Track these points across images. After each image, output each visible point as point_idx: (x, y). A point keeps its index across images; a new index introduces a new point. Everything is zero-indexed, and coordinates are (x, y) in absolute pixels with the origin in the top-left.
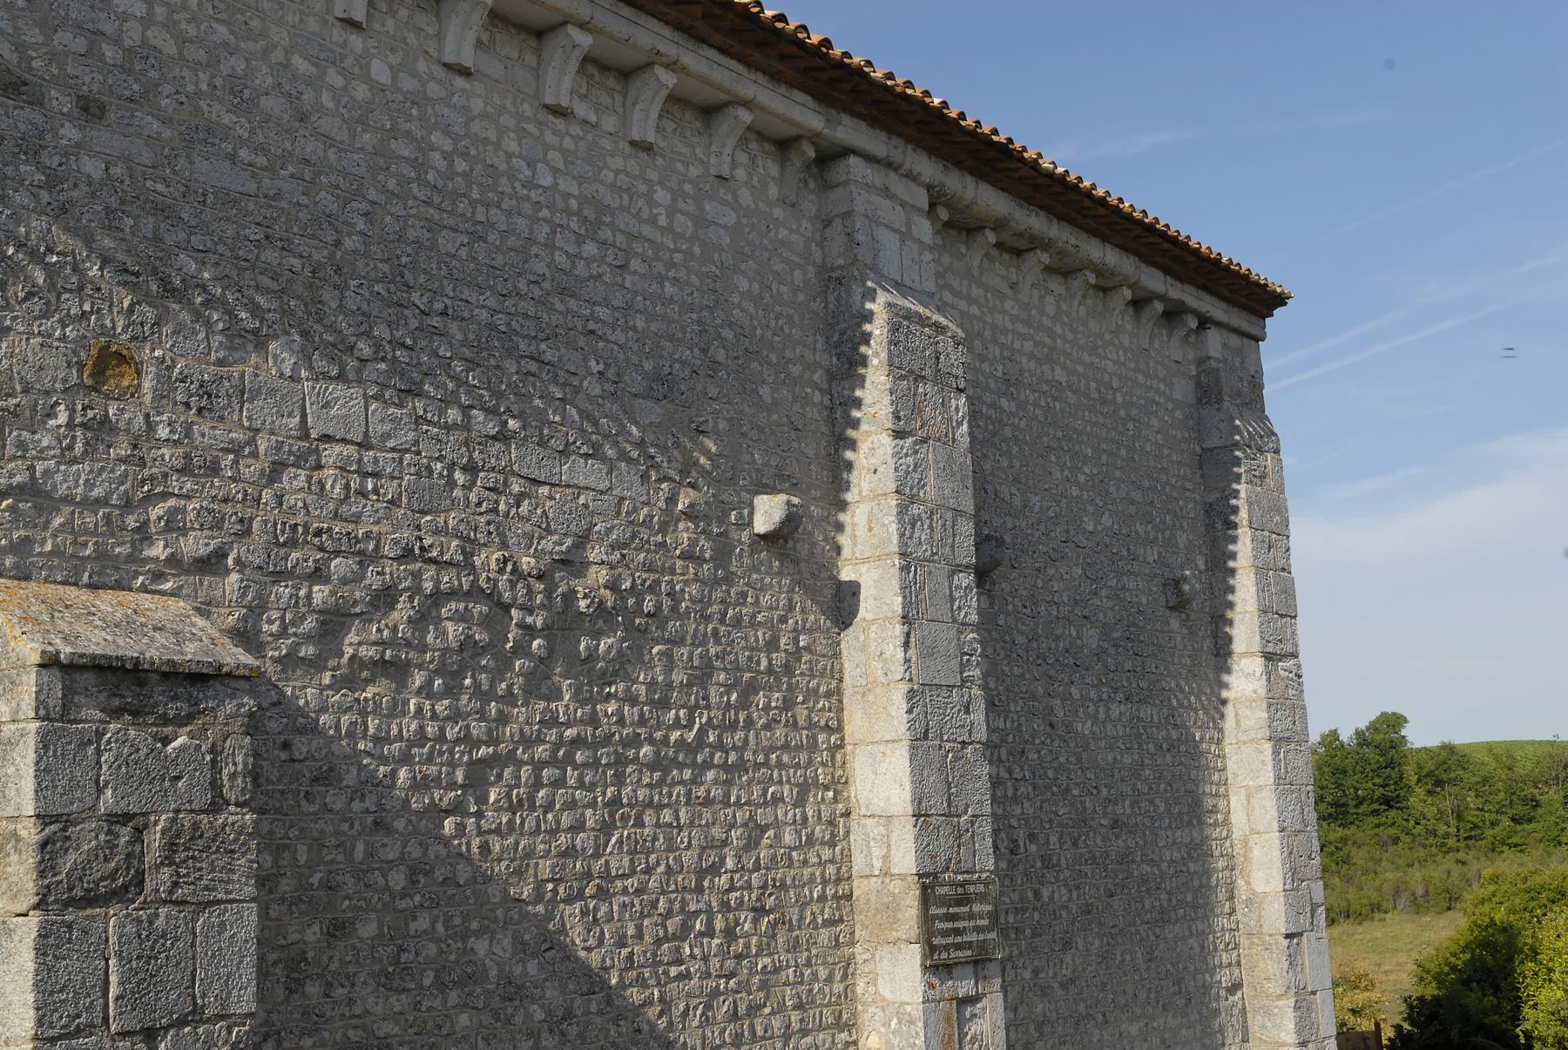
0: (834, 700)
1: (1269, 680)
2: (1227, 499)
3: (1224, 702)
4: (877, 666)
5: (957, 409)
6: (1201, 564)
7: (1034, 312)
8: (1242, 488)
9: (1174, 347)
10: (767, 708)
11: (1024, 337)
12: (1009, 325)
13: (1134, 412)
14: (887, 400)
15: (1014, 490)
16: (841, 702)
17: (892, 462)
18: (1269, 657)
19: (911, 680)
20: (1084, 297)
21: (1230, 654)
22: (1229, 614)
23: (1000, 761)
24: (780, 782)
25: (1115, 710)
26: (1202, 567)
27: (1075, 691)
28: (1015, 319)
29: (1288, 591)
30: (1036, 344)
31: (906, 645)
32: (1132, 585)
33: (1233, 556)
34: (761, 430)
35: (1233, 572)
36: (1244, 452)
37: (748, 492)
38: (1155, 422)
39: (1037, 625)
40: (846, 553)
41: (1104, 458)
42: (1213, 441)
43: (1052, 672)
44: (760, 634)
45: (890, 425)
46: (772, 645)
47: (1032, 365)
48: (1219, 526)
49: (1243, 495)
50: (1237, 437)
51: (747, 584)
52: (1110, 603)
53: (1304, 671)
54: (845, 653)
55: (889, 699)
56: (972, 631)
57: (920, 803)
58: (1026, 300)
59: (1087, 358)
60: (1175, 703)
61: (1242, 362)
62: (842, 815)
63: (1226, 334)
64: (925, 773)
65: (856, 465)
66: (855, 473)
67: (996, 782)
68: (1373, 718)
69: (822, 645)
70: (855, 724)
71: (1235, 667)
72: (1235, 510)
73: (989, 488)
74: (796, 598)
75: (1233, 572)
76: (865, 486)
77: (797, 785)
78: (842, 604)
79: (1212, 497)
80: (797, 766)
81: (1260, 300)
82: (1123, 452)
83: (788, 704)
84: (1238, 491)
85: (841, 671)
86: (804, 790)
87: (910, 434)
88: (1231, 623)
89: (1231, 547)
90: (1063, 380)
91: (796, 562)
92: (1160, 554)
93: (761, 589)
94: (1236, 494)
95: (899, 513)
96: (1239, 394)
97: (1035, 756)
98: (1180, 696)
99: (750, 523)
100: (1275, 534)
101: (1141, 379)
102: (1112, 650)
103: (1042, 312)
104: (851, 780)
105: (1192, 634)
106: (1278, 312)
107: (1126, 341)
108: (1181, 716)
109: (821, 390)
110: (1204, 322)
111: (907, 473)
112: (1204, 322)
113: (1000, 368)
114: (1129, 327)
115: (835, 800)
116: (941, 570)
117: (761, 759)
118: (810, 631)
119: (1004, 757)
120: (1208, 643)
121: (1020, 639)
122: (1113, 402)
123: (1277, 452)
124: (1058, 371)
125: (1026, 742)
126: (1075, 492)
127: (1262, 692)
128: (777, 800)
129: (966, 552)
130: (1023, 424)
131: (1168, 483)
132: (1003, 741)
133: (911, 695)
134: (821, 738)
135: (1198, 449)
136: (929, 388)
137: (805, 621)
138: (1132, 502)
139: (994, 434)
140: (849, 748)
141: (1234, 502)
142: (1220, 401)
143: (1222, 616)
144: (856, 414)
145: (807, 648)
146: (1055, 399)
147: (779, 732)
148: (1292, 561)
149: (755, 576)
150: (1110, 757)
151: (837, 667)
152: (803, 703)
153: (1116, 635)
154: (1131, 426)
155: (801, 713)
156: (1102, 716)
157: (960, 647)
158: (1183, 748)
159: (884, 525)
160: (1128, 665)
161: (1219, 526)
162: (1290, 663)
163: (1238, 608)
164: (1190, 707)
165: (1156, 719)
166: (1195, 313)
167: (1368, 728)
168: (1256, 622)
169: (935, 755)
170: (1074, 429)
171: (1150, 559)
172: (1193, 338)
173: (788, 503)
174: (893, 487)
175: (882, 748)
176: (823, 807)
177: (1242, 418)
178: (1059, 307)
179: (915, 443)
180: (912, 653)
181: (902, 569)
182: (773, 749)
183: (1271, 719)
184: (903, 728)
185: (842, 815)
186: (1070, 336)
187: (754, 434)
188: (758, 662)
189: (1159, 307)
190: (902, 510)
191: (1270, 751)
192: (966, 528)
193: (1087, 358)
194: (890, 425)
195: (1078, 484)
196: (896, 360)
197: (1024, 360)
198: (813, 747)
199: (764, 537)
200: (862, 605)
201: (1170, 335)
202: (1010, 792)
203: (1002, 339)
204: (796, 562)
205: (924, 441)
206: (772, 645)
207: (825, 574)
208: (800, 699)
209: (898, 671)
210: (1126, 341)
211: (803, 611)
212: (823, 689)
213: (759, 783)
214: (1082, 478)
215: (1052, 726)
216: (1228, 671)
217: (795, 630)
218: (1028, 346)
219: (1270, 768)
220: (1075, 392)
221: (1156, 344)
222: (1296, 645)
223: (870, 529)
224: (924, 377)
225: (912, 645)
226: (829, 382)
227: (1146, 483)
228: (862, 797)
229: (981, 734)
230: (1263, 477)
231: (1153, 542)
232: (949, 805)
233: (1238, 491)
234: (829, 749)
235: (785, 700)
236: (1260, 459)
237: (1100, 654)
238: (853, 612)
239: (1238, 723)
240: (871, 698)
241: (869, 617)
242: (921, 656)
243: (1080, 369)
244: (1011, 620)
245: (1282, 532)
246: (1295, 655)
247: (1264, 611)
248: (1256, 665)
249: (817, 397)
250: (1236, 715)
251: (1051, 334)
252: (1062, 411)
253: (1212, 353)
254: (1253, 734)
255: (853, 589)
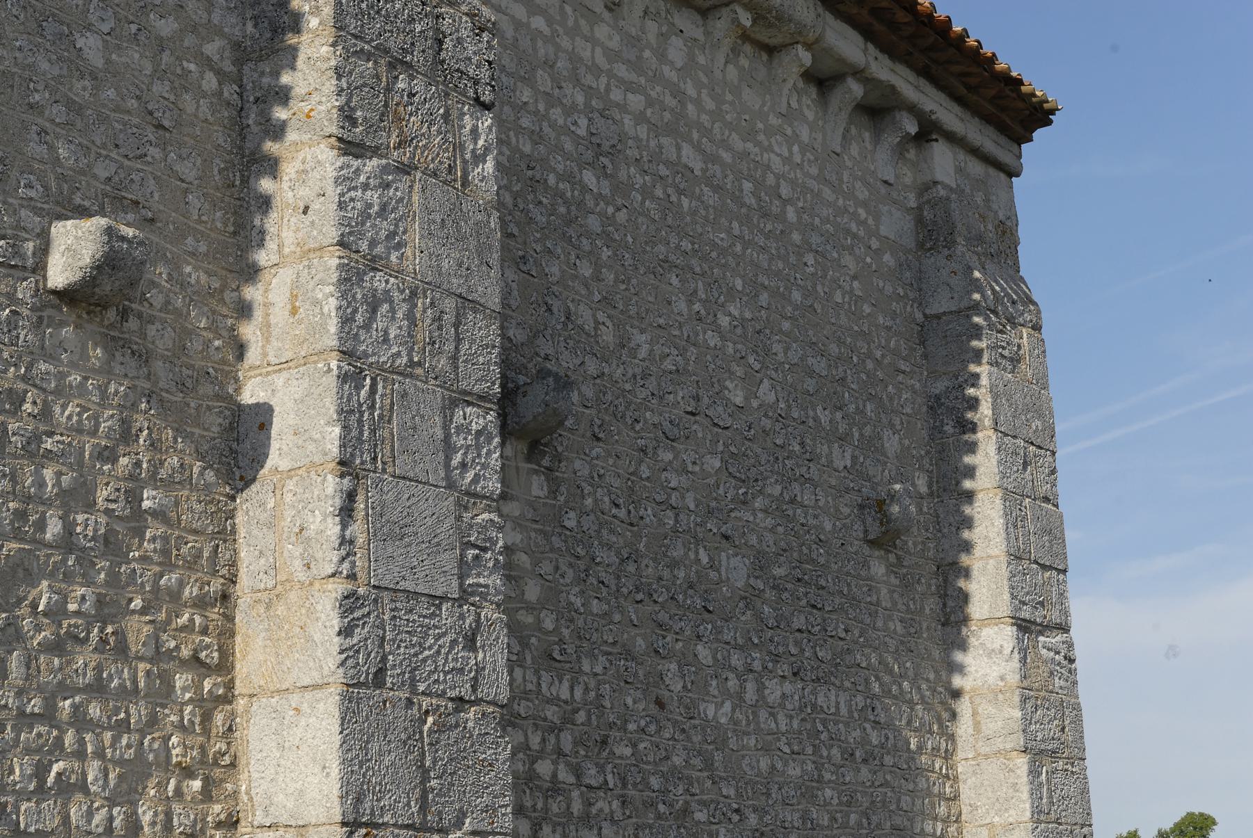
0: (214, 613)
1: (1023, 660)
2: (961, 387)
3: (957, 694)
4: (293, 551)
5: (475, 132)
6: (922, 485)
7: (647, 54)
8: (983, 370)
9: (877, 158)
10: (56, 613)
11: (630, 87)
12: (601, 60)
13: (815, 240)
14: (330, 85)
15: (601, 316)
16: (230, 619)
17: (333, 193)
18: (1024, 626)
19: (352, 577)
20: (735, 51)
21: (966, 620)
22: (964, 559)
23: (560, 753)
24: (80, 754)
25: (774, 691)
26: (924, 489)
27: (703, 652)
28: (613, 56)
29: (1054, 533)
30: (650, 103)
31: (346, 513)
32: (807, 498)
33: (970, 472)
34: (70, 105)
35: (969, 496)
36: (987, 318)
37: (37, 211)
38: (848, 260)
39: (638, 536)
40: (252, 356)
41: (764, 298)
42: (941, 304)
43: (663, 616)
44: (48, 474)
45: (334, 129)
46: (77, 497)
47: (642, 132)
48: (949, 429)
49: (984, 381)
50: (977, 296)
51: (24, 379)
52: (769, 522)
53: (1078, 653)
54: (242, 532)
55: (311, 611)
56: (488, 509)
57: (359, 800)
58: (633, 31)
59: (739, 145)
60: (876, 688)
61: (987, 201)
62: (219, 825)
63: (962, 156)
64: (374, 747)
65: (277, 202)
66: (274, 215)
67: (525, 781)
68: (1177, 819)
69: (192, 510)
70: (253, 660)
71: (973, 641)
72: (974, 404)
73: (556, 305)
74: (140, 421)
75: (969, 496)
76: (288, 236)
77: (121, 762)
78: (239, 445)
79: (939, 387)
80: (123, 726)
81: (1015, 112)
82: (797, 296)
83: (107, 609)
84: (977, 376)
85: (233, 564)
86: (133, 778)
87: (375, 151)
88: (966, 573)
89: (968, 459)
90: (697, 166)
91: (144, 358)
92: (854, 458)
93: (58, 392)
94: (974, 379)
95: (342, 281)
96: (980, 239)
97: (628, 751)
98: (887, 679)
99: (40, 267)
100: (1033, 447)
101: (828, 193)
102: (770, 594)
103: (662, 57)
104: (242, 761)
105: (907, 585)
106: (1039, 134)
107: (805, 135)
108: (886, 709)
109: (219, 73)
110: (928, 131)
111: (365, 215)
112: (928, 131)
113: (583, 122)
114: (810, 115)
115: (207, 795)
116: (431, 397)
117: (35, 705)
118: (168, 484)
119: (567, 747)
120: (931, 605)
121: (602, 555)
122: (781, 217)
123: (1037, 328)
124: (687, 150)
125: (611, 726)
126: (713, 340)
127: (1014, 679)
128: (68, 788)
129: (482, 372)
130: (622, 216)
131: (869, 355)
132: (568, 720)
133: (349, 603)
134: (181, 680)
135: (919, 316)
136: (418, 85)
137: (156, 466)
138: (811, 373)
139: (569, 222)
140: (241, 703)
141: (971, 391)
142: (950, 244)
143: (955, 564)
144: (281, 114)
145: (159, 514)
146: (681, 192)
147: (84, 659)
148: (1060, 488)
149: (43, 367)
150: (764, 764)
151: (224, 555)
152: (144, 611)
153: (779, 572)
154: (810, 259)
155: (138, 631)
156: (750, 695)
157: (462, 532)
158: (888, 760)
159: (316, 303)
160: (799, 622)
161: (949, 429)
162: (1057, 639)
163: (978, 551)
164: (900, 697)
165: (844, 711)
166: (913, 109)
167: (1173, 831)
168: (1005, 573)
169: (399, 718)
170: (714, 245)
171: (840, 464)
172: (912, 154)
173: (109, 231)
174: (333, 234)
175: (295, 699)
176: (177, 808)
177: (983, 269)
178: (691, 58)
179: (385, 170)
180: (357, 529)
181: (343, 378)
182: (65, 690)
183: (1027, 721)
184: (332, 662)
185: (219, 825)
186: (710, 104)
187: (58, 112)
188: (41, 525)
189: (856, 89)
190: (348, 279)
191: (1025, 769)
192: (483, 335)
193: (739, 145)
194: (334, 129)
195: (718, 329)
196: (353, 25)
197: (628, 122)
198: (163, 693)
199: (67, 296)
200: (275, 445)
201: (877, 140)
202: (577, 807)
203: (589, 80)
204: (144, 358)
205: (405, 169)
206: (77, 497)
207: (207, 389)
208: (137, 603)
209: (328, 559)
210: (805, 135)
211: (153, 445)
212: (189, 592)
213: (28, 751)
214: (724, 321)
215: (660, 704)
216: (963, 646)
217: (132, 477)
218: (636, 101)
219: (1025, 795)
220: (717, 189)
221: (854, 150)
222: (1066, 613)
223: (294, 311)
224: (409, 66)
225: (360, 513)
226: (239, 63)
227: (834, 348)
228: (258, 792)
229: (498, 686)
230: (1015, 360)
231: (843, 439)
232: (424, 808)
233: (977, 376)
234: (198, 701)
235: (100, 601)
236: (1011, 334)
237: (749, 598)
238: (259, 459)
239: (977, 725)
240: (281, 610)
241: (284, 465)
242: (372, 536)
243: (726, 156)
244: (588, 523)
245: (1044, 443)
246: (1064, 628)
247: (1016, 556)
248: (1002, 637)
249: (210, 82)
250: (975, 714)
251: (678, 93)
252: (694, 213)
253: (939, 177)
254: (999, 744)
255: (262, 416)
